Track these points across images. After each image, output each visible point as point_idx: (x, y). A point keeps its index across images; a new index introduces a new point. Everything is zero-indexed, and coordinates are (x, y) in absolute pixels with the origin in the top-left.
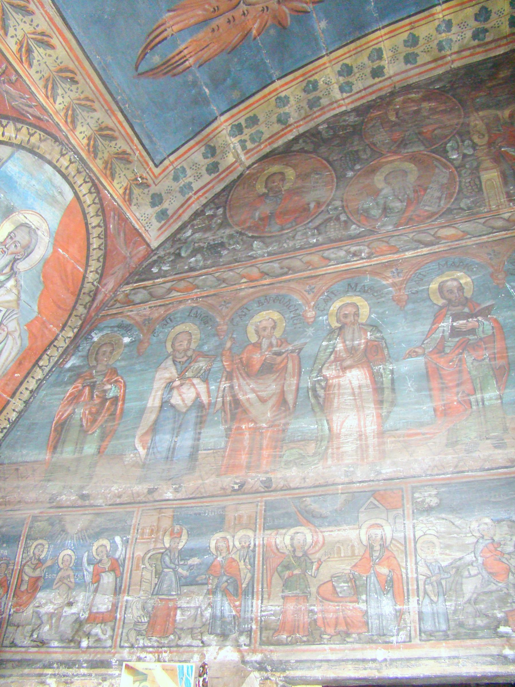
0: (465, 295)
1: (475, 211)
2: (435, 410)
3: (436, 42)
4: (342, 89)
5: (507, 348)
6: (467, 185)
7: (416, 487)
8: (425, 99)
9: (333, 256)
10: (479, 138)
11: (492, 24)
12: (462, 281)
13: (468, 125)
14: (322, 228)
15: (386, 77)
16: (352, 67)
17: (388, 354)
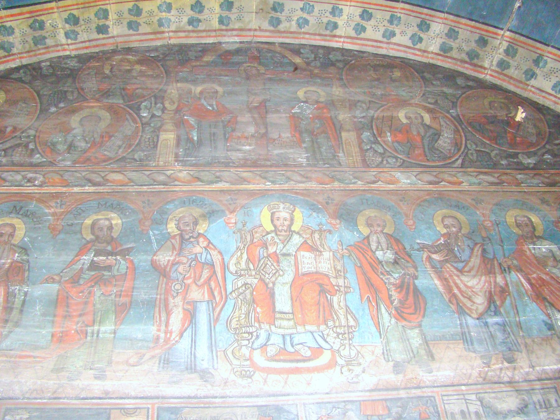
0: (113, 234)
1: (145, 163)
2: (53, 336)
3: (157, 18)
4: (67, 35)
5: (133, 288)
6: (147, 140)
7: (10, 409)
8: (139, 62)
9: (10, 178)
10: (169, 103)
11: (205, 17)
12: (114, 222)
13: (166, 91)
14: (10, 152)
15: (110, 35)
16: (78, 18)
17: (28, 276)
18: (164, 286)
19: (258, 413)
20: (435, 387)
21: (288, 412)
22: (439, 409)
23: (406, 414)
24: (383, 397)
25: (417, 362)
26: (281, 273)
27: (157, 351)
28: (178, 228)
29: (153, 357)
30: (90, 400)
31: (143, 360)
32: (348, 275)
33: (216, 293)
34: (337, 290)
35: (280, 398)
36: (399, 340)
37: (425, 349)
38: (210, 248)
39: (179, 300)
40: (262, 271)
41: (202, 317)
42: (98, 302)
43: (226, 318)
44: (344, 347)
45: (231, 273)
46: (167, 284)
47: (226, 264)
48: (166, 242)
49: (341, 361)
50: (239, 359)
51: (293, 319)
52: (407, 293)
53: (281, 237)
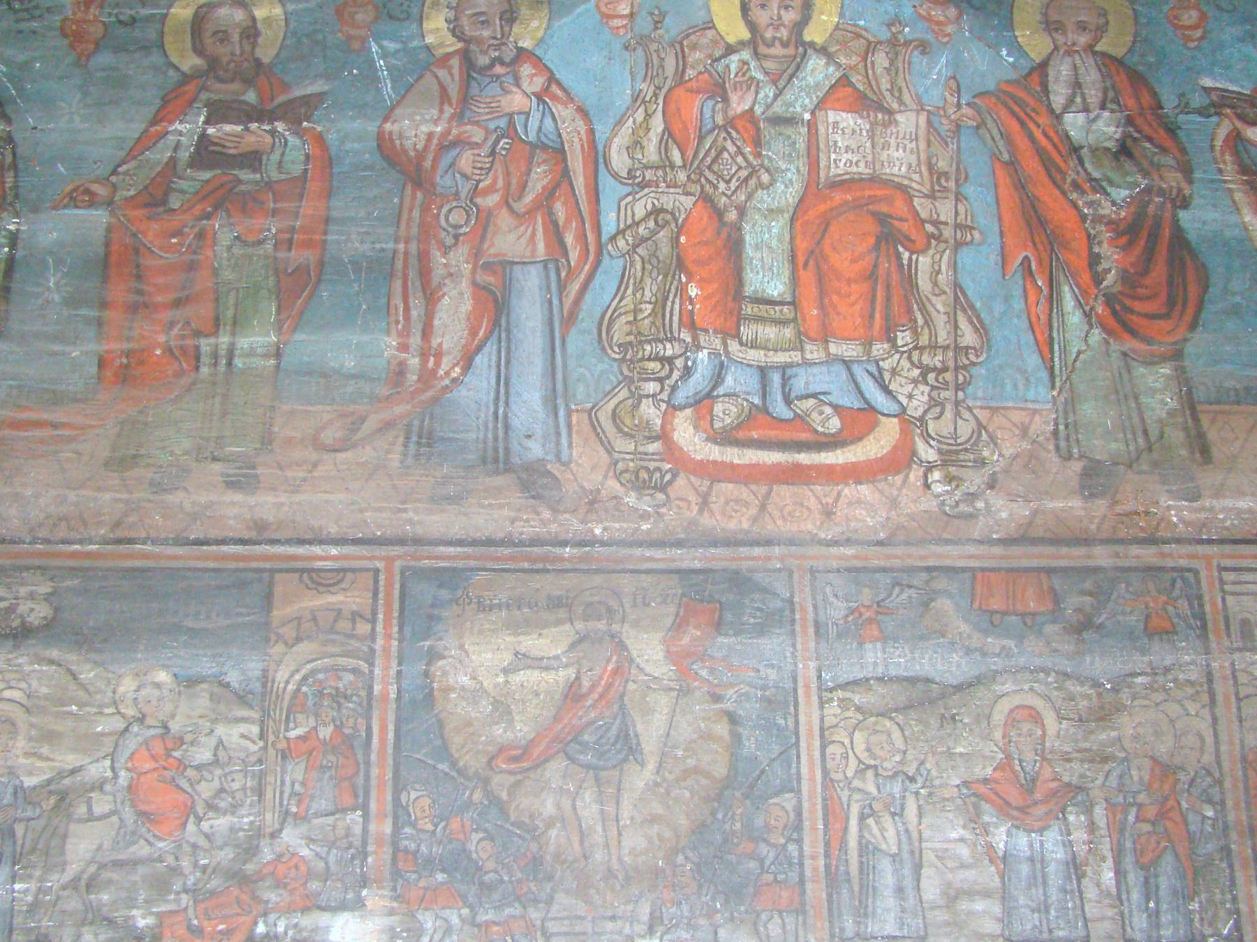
0: (259, 53)
2: (102, 363)
5: (327, 221)
17: (16, 187)
18: (416, 214)
19: (680, 591)
20: (1201, 542)
21: (765, 590)
22: (1207, 608)
23: (1104, 616)
24: (1044, 563)
25: (1155, 464)
26: (765, 178)
27: (399, 410)
28: (457, 32)
29: (388, 425)
30: (215, 548)
31: (359, 435)
32: (968, 190)
33: (569, 239)
34: (932, 236)
35: (743, 551)
36: (1106, 397)
37: (1186, 429)
38: (554, 98)
39: (460, 259)
40: (707, 173)
41: (529, 313)
42: (225, 262)
43: (598, 315)
44: (938, 409)
45: (615, 176)
46: (425, 209)
47: (600, 148)
48: (420, 77)
49: (927, 453)
50: (633, 437)
51: (794, 320)
52: (1149, 254)
53: (769, 65)
